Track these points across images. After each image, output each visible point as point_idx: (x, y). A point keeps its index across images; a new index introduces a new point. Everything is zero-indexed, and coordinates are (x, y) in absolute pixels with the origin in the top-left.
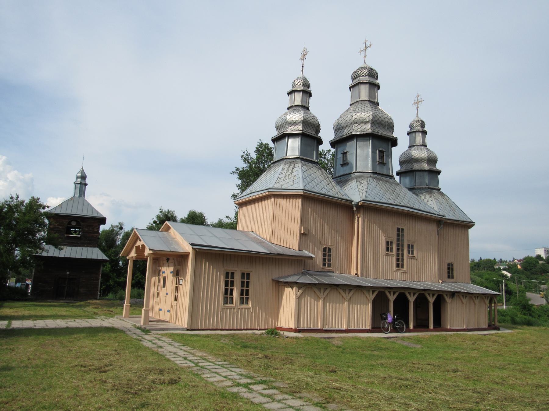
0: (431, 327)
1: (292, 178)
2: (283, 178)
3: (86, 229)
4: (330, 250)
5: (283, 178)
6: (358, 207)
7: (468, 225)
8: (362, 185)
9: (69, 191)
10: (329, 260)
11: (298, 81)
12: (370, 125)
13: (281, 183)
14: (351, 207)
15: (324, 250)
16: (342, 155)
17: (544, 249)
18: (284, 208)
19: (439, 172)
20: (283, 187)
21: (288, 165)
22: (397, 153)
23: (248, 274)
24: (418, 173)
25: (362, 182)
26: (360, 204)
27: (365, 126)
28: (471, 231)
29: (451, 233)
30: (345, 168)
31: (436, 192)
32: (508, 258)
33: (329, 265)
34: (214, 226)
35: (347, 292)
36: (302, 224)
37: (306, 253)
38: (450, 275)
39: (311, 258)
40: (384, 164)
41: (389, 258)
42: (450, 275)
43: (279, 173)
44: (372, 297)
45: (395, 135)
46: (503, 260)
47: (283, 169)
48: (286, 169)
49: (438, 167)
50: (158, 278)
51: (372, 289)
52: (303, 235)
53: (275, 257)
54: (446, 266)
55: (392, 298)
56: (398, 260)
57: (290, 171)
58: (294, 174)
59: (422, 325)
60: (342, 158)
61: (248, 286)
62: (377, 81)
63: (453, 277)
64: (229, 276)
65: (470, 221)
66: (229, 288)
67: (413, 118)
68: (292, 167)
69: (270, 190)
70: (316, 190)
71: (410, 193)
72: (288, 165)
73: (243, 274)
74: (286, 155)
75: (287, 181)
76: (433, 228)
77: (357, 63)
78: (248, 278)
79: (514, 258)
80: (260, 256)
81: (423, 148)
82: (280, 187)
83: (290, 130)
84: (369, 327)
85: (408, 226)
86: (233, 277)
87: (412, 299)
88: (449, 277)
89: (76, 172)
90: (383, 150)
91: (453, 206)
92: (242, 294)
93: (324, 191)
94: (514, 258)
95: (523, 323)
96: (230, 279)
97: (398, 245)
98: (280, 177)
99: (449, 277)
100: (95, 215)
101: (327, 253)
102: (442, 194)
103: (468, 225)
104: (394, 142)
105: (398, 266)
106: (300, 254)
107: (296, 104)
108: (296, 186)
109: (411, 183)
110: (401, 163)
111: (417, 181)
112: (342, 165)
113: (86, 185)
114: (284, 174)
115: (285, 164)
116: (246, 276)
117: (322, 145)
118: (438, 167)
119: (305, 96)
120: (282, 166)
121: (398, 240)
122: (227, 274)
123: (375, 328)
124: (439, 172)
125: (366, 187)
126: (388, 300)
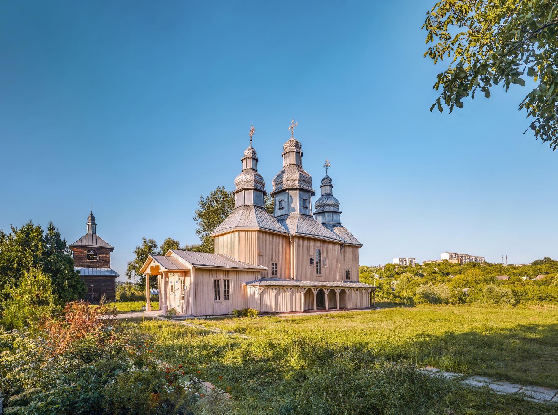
1: (250, 219)
2: (244, 219)
3: (101, 256)
4: (276, 264)
5: (244, 219)
6: (293, 237)
7: (358, 246)
8: (294, 222)
9: (86, 230)
11: (249, 151)
12: (297, 182)
13: (243, 223)
14: (288, 237)
15: (273, 264)
16: (279, 202)
17: (399, 259)
18: (246, 239)
20: (245, 226)
21: (246, 210)
22: (314, 200)
23: (228, 281)
24: (327, 213)
25: (294, 220)
26: (294, 235)
27: (294, 183)
30: (281, 211)
32: (376, 265)
33: (276, 274)
34: (185, 250)
36: (259, 248)
37: (262, 267)
38: (348, 278)
39: (266, 270)
40: (307, 208)
41: (312, 268)
42: (348, 278)
43: (240, 216)
45: (313, 188)
46: (373, 266)
47: (243, 213)
48: (245, 213)
49: (340, 209)
52: (260, 256)
53: (243, 270)
55: (315, 292)
56: (317, 269)
57: (248, 214)
58: (251, 216)
59: (334, 308)
60: (279, 205)
61: (228, 288)
62: (301, 151)
63: (349, 279)
65: (359, 244)
66: (217, 290)
68: (249, 211)
69: (236, 227)
70: (266, 227)
71: (323, 227)
72: (246, 210)
73: (225, 281)
74: (244, 204)
75: (247, 221)
76: (338, 248)
79: (380, 265)
80: (217, 269)
81: (330, 196)
82: (243, 226)
83: (245, 186)
84: (302, 310)
85: (323, 247)
87: (327, 292)
88: (347, 278)
89: (89, 214)
90: (306, 199)
91: (349, 234)
93: (271, 227)
94: (380, 265)
95: (205, 333)
96: (217, 285)
98: (242, 218)
99: (347, 278)
100: (106, 246)
101: (274, 266)
102: (342, 226)
103: (358, 246)
104: (313, 194)
105: (317, 273)
106: (258, 267)
107: (248, 167)
108: (253, 225)
109: (323, 220)
110: (316, 207)
111: (327, 219)
112: (279, 209)
113: (96, 225)
114: (244, 216)
115: (244, 210)
118: (340, 209)
119: (254, 161)
120: (242, 211)
122: (215, 281)
123: (306, 311)
125: (297, 224)
126: (313, 293)
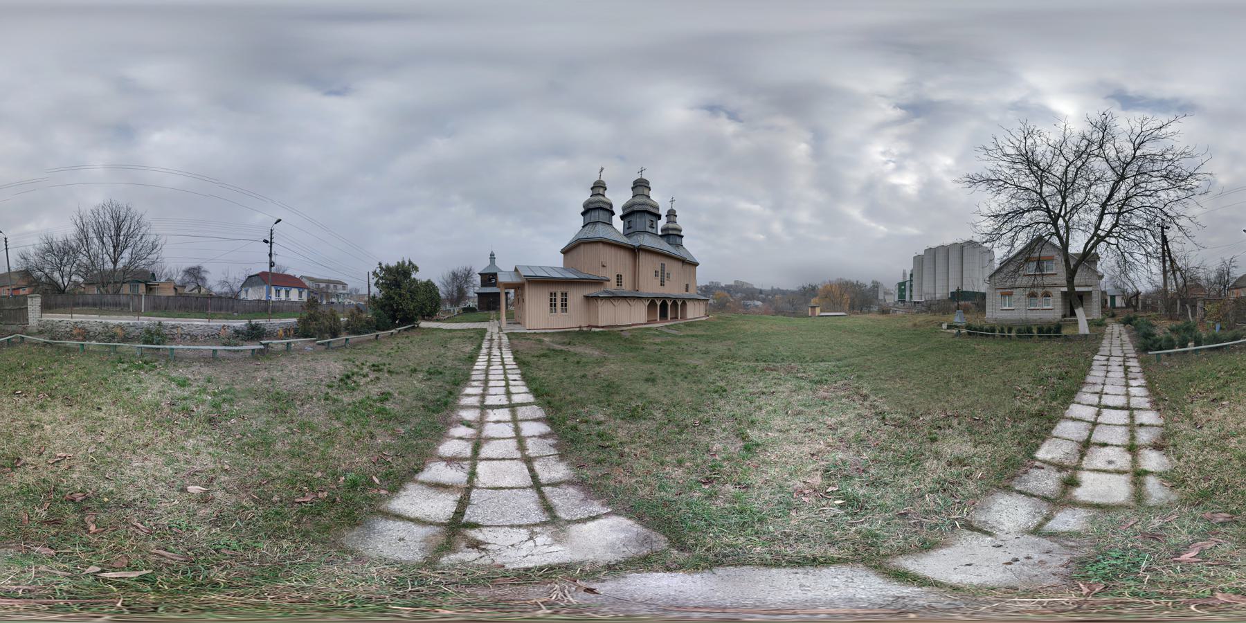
0: (669, 319)
9: (488, 262)
10: (621, 282)
15: (618, 276)
19: (682, 237)
23: (566, 294)
24: (671, 237)
28: (697, 267)
29: (687, 268)
31: (680, 247)
33: (621, 285)
35: (616, 301)
42: (687, 291)
44: (647, 303)
45: (660, 212)
50: (482, 379)
51: (648, 298)
54: (616, 278)
64: (553, 294)
66: (553, 303)
67: (670, 208)
77: (638, 177)
78: (566, 296)
85: (667, 262)
86: (555, 295)
92: (562, 306)
97: (661, 273)
104: (659, 217)
105: (661, 285)
110: (662, 231)
116: (564, 294)
117: (432, 280)
118: (682, 234)
121: (662, 270)
122: (551, 294)
124: (682, 237)
126: (656, 305)
